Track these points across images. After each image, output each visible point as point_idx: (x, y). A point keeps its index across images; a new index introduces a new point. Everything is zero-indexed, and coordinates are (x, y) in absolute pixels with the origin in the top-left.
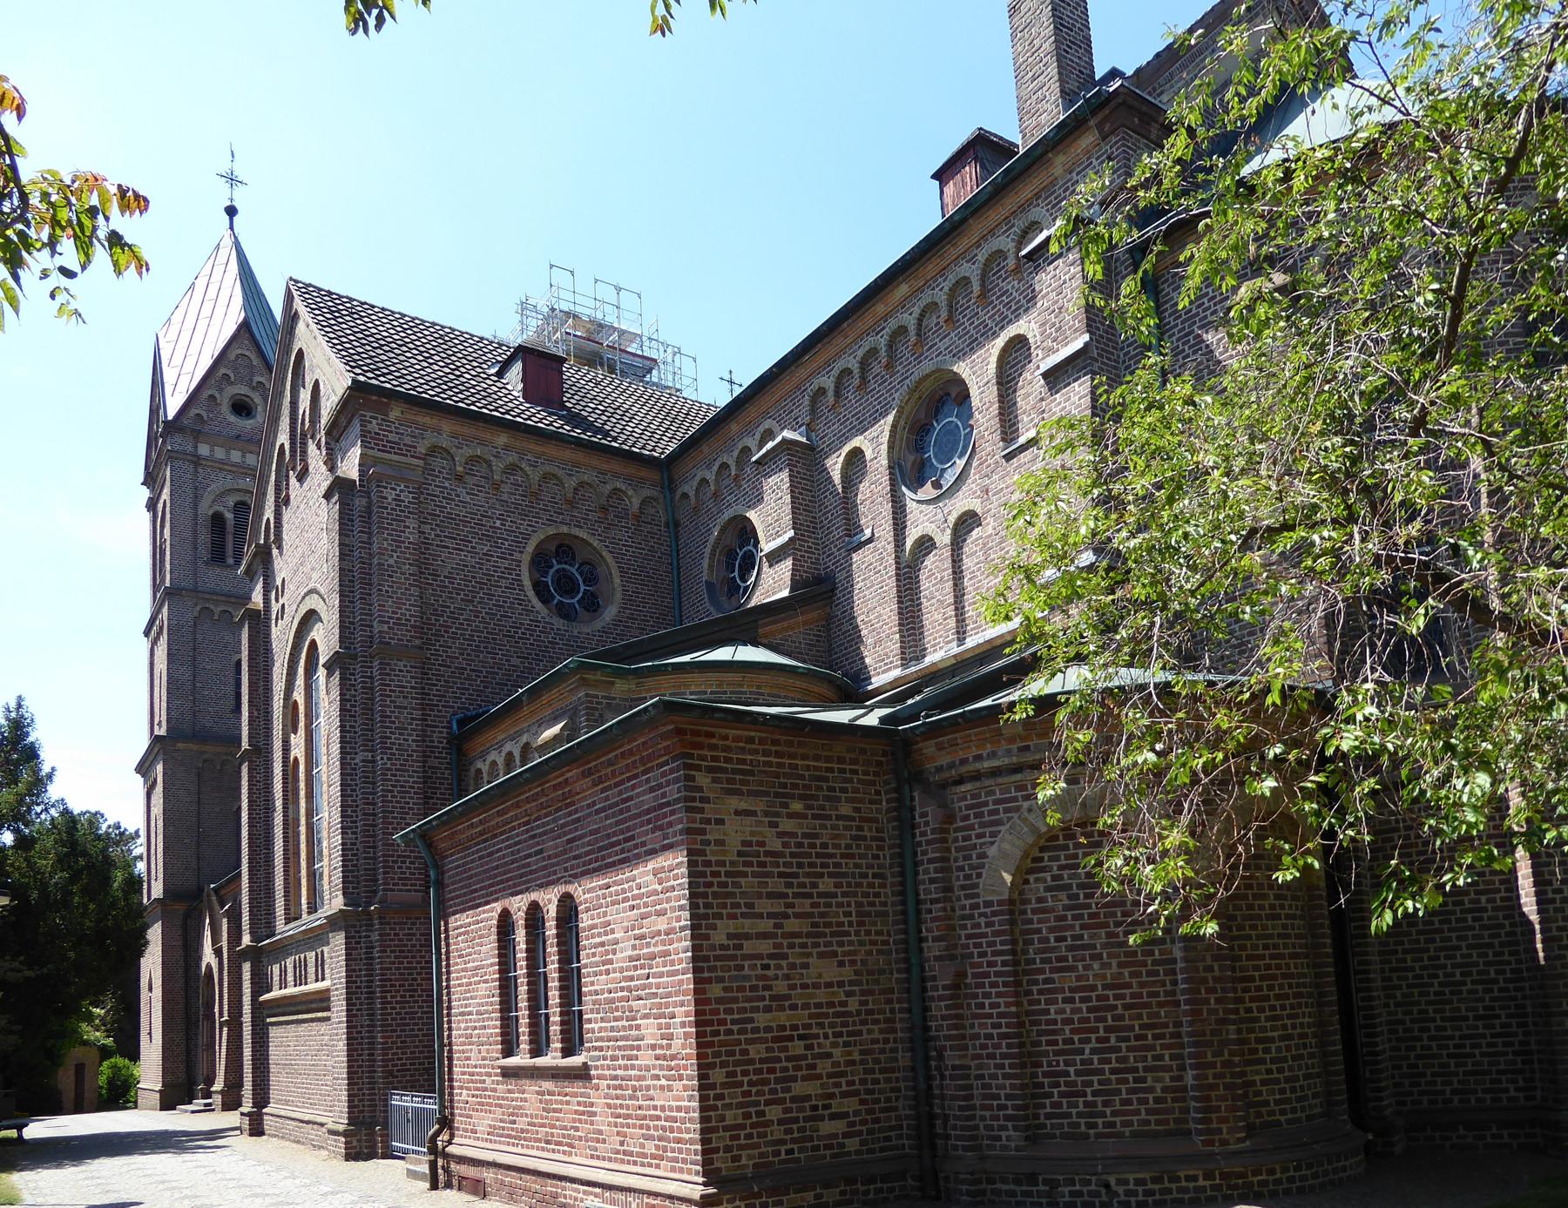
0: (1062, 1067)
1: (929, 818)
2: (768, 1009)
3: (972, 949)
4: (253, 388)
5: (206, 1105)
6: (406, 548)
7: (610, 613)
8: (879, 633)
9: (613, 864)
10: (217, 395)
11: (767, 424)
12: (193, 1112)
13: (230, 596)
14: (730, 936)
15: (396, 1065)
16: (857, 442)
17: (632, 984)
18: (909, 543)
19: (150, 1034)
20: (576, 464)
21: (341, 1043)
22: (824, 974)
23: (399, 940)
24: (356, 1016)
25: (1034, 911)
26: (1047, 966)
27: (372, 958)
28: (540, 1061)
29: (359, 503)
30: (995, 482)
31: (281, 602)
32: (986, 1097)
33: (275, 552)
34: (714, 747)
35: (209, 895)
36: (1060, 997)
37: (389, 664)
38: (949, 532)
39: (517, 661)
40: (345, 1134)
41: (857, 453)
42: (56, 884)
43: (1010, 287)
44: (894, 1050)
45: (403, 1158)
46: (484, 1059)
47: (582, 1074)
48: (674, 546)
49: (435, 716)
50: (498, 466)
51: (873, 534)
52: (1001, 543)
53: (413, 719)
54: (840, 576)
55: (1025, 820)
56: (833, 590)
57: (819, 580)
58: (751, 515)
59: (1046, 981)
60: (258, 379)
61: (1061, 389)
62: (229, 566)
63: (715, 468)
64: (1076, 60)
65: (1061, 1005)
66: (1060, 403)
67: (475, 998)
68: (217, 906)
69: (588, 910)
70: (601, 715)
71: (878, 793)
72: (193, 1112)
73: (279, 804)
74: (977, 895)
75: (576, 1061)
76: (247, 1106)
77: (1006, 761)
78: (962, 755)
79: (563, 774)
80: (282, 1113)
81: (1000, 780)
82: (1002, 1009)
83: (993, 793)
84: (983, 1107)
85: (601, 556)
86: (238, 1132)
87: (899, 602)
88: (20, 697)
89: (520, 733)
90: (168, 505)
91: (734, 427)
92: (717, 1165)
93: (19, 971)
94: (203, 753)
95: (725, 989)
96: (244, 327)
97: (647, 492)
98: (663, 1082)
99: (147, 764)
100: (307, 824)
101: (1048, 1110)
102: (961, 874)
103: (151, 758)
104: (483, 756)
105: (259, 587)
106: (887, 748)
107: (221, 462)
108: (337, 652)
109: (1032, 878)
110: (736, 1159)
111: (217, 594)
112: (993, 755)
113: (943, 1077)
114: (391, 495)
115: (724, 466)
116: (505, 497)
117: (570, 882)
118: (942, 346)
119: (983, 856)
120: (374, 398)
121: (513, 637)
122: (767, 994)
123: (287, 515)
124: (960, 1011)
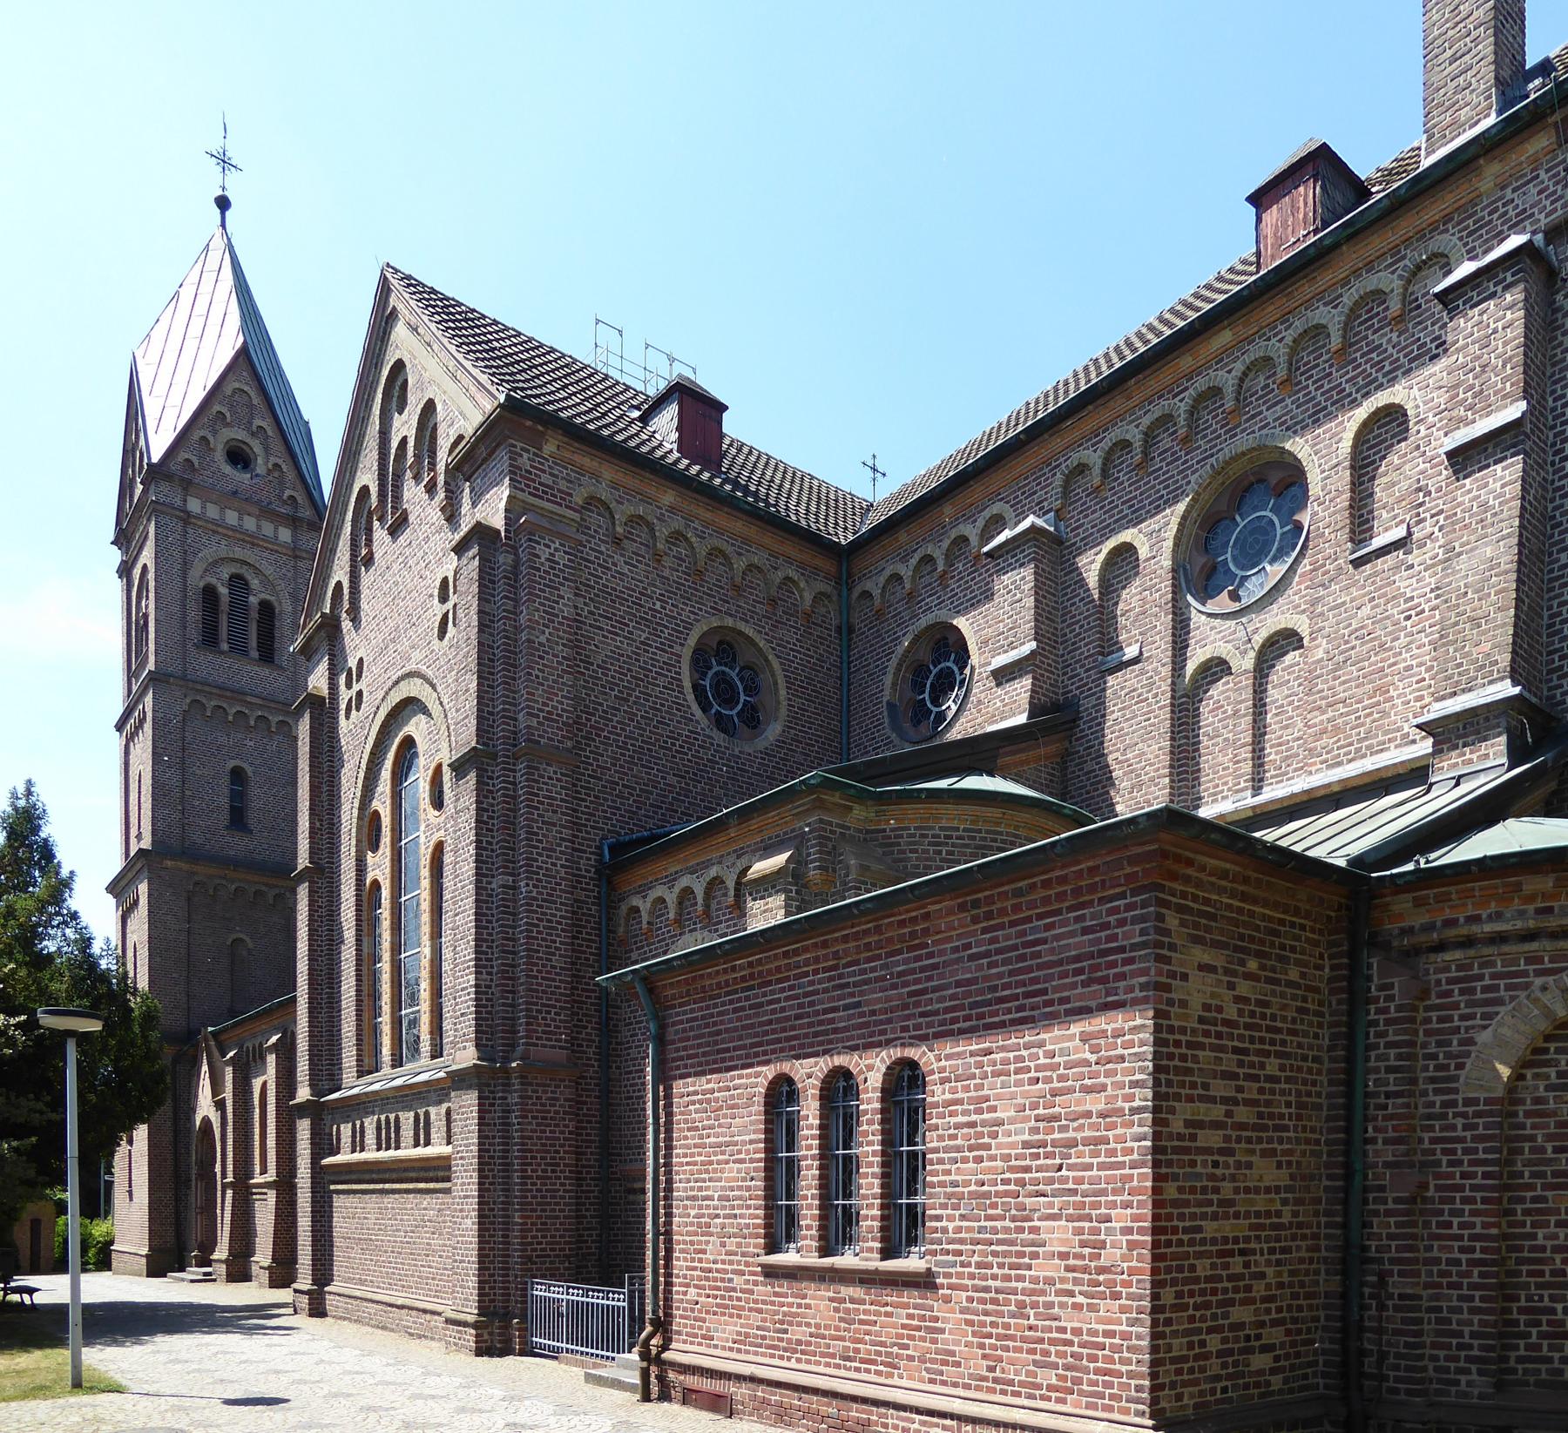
0: (1546, 1302)
1: (1396, 991)
2: (1215, 1217)
3: (1439, 1156)
4: (253, 434)
5: (205, 1274)
6: (559, 623)
7: (773, 731)
8: (1140, 775)
9: (1002, 1025)
10: (211, 439)
11: (996, 508)
14: (1189, 1124)
15: (536, 1250)
16: (1126, 536)
17: (1027, 1176)
18: (1191, 667)
21: (469, 1221)
22: (1265, 1178)
23: (542, 1105)
24: (489, 1190)
25: (1528, 1114)
26: (1539, 1182)
27: (508, 1124)
28: (846, 1260)
29: (504, 559)
30: (1336, 593)
31: (356, 687)
32: (1439, 1333)
33: (346, 625)
34: (1187, 880)
35: (206, 1040)
36: (1553, 1219)
37: (537, 769)
38: (1252, 654)
39: (672, 780)
40: (475, 1326)
41: (1126, 552)
43: (1384, 341)
44: (1317, 1272)
45: (556, 1358)
46: (728, 1253)
47: (924, 1282)
48: (845, 658)
49: (583, 838)
50: (662, 532)
51: (1141, 653)
52: (1336, 670)
53: (562, 839)
54: (1087, 703)
55: (1536, 1001)
56: (1075, 720)
57: (1056, 707)
58: (961, 623)
59: (1535, 1200)
60: (258, 422)
61: (1474, 472)
62: (222, 653)
63: (914, 561)
64: (1511, 39)
65: (1552, 1229)
66: (1470, 491)
67: (720, 1180)
68: (216, 1053)
69: (943, 1081)
70: (834, 848)
71: (1321, 957)
73: (349, 934)
74: (1456, 1091)
75: (912, 1262)
76: (304, 1282)
77: (1519, 924)
78: (1448, 914)
79: (924, 907)
80: (358, 1294)
81: (1506, 948)
82: (1478, 1230)
83: (1493, 964)
84: (1434, 1346)
85: (767, 660)
86: (291, 1311)
87: (1173, 739)
89: (707, 865)
90: (151, 576)
91: (948, 510)
92: (1163, 1404)
93: (41, 1113)
94: (194, 873)
95: (1181, 1190)
96: (243, 355)
97: (821, 586)
98: (1080, 1299)
100: (393, 961)
101: (1522, 1352)
102: (1432, 1064)
103: (130, 875)
104: (642, 891)
105: (322, 668)
106: (1343, 901)
107: (213, 522)
108: (474, 748)
109: (1529, 1073)
110: (1179, 1397)
112: (1498, 916)
113: (1382, 1307)
114: (544, 553)
115: (928, 559)
116: (666, 573)
117: (911, 1045)
118: (1270, 416)
119: (1471, 1042)
120: (529, 423)
121: (671, 750)
122: (1215, 1197)
123: (367, 579)
124: (1415, 1230)
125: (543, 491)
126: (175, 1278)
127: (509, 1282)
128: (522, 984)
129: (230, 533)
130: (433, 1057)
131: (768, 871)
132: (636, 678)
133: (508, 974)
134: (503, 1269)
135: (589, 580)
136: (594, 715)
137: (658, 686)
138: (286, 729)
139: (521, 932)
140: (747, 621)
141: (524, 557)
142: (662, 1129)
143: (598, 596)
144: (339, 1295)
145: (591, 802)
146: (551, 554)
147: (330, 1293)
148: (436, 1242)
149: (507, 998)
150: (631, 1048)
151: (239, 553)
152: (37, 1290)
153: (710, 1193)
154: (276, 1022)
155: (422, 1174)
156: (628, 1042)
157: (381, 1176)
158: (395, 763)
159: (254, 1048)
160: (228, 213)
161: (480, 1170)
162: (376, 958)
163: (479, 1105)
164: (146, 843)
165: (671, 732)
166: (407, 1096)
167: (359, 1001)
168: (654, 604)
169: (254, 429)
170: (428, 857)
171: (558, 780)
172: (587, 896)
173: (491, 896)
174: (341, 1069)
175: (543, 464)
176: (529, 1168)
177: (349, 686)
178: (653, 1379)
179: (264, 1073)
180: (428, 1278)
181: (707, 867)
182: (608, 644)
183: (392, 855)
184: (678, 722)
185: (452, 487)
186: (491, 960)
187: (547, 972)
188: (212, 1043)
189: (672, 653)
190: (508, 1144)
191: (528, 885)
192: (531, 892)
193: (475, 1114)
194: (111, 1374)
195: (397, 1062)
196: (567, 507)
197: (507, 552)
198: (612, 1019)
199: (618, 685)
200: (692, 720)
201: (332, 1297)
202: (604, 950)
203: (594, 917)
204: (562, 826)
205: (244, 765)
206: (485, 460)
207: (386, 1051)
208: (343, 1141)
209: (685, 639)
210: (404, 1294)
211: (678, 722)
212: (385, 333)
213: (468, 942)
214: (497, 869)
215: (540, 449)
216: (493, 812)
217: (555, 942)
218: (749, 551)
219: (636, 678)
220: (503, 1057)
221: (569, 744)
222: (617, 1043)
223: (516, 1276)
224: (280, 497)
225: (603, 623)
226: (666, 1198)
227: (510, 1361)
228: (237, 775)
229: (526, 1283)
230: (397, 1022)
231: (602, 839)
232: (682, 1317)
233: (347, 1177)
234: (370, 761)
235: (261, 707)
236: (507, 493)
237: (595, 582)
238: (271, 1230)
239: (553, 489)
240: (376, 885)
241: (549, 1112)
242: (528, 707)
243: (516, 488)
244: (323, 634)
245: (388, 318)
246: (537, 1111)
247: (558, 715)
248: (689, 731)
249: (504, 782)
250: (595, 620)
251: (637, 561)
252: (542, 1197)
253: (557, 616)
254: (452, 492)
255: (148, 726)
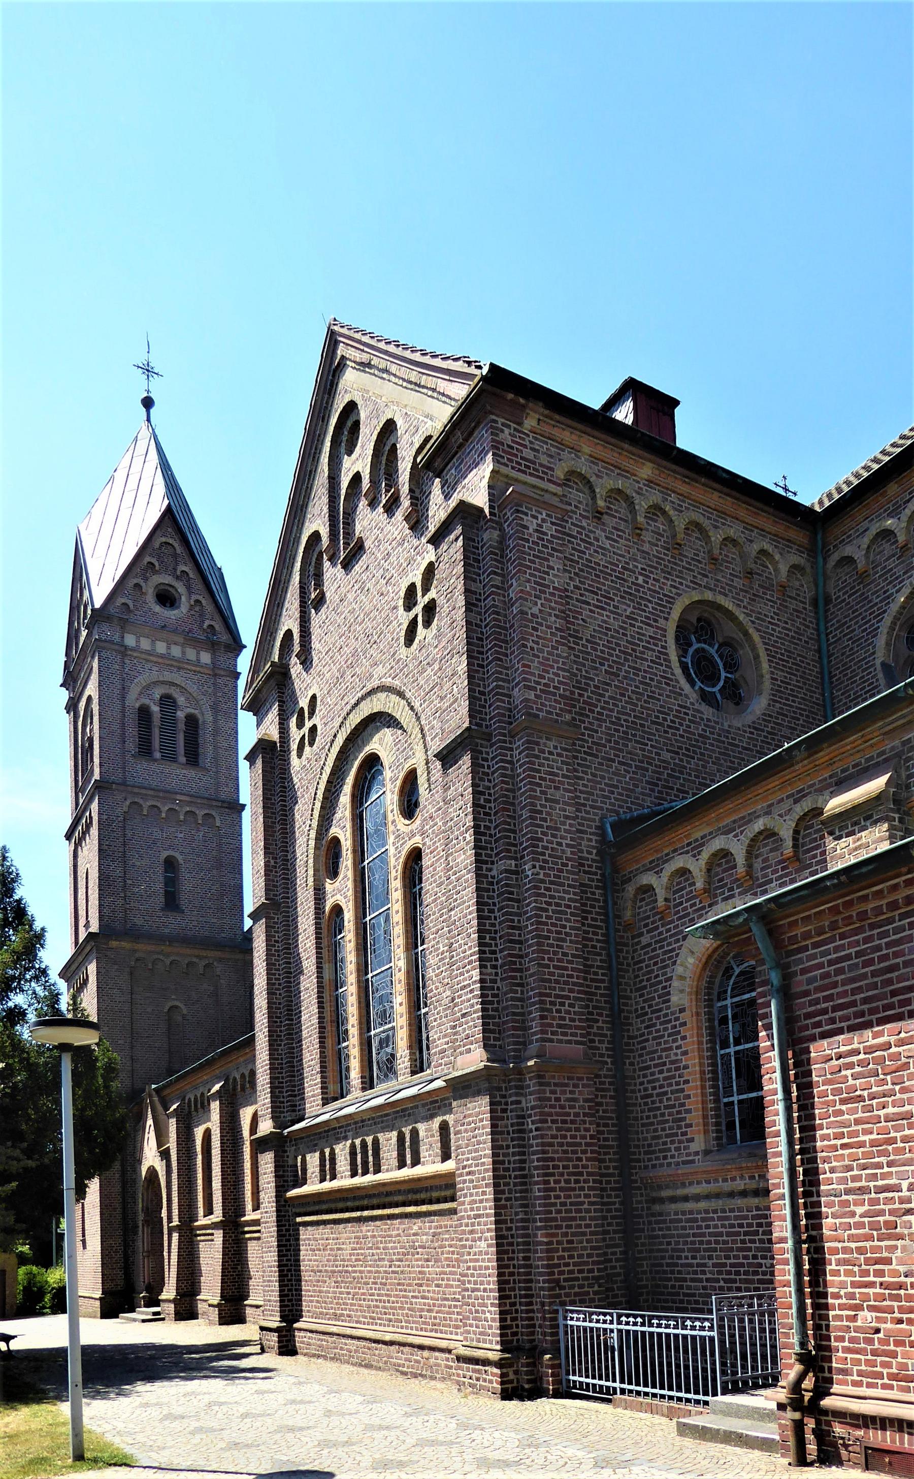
5: (155, 1314)
6: (550, 594)
7: (759, 705)
10: (143, 584)
12: (144, 1321)
13: (159, 791)
19: (84, 1242)
20: (723, 513)
21: (483, 1245)
24: (505, 1207)
29: (490, 536)
31: (308, 724)
33: (296, 669)
35: (150, 1096)
37: (538, 744)
39: (667, 756)
40: (499, 1364)
42: (46, 1063)
45: (609, 1401)
50: (642, 505)
53: (567, 817)
62: (156, 760)
68: (160, 1108)
72: (144, 1321)
73: (309, 963)
80: (334, 1329)
85: (746, 634)
88: (4, 847)
90: (95, 707)
93: (19, 1160)
94: (135, 951)
96: (168, 513)
97: (795, 559)
99: (74, 967)
103: (80, 959)
104: (655, 867)
111: (145, 788)
114: (532, 525)
116: (646, 547)
120: (511, 396)
123: (316, 619)
125: (526, 466)
126: (127, 1319)
127: (533, 1311)
128: (531, 975)
129: (160, 660)
130: (413, 1073)
131: (861, 800)
132: (624, 653)
133: (515, 966)
134: (526, 1296)
135: (573, 555)
136: (586, 690)
137: (646, 660)
138: (211, 820)
139: (528, 919)
140: (726, 595)
141: (509, 531)
142: (795, 1106)
143: (582, 571)
144: (311, 1331)
145: (588, 780)
146: (538, 525)
147: (300, 1330)
148: (431, 1270)
149: (516, 992)
150: (647, 1040)
151: (168, 676)
152: (13, 1337)
153: (893, 1181)
154: (217, 1072)
155: (410, 1197)
156: (643, 1035)
157: (357, 1203)
158: (355, 786)
159: (196, 1099)
160: (152, 411)
161: (496, 1185)
162: (338, 983)
163: (491, 1111)
164: (94, 928)
165: (661, 706)
166: (386, 1115)
167: (322, 1028)
168: (637, 579)
169: (178, 573)
170: (400, 868)
171: (559, 755)
172: (589, 879)
173: (492, 883)
174: (303, 1099)
175: (524, 439)
176: (552, 1179)
177: (300, 725)
178: (809, 1436)
179: (209, 1120)
180: (422, 1310)
181: (750, 821)
182: (595, 619)
183: (355, 876)
184: (668, 696)
185: (417, 494)
186: (494, 952)
187: (559, 960)
188: (156, 1099)
189: (657, 627)
190: (524, 1154)
191: (534, 867)
192: (538, 874)
193: (487, 1123)
194: (109, 1438)
195: (368, 1083)
196: (549, 481)
197: (493, 528)
198: (623, 1011)
199: (608, 660)
200: (681, 695)
201: (302, 1334)
202: (612, 935)
203: (598, 901)
204: (565, 803)
205: (177, 855)
206: (460, 446)
207: (355, 1075)
208: (309, 1172)
209: (669, 613)
210: (390, 1329)
211: (668, 696)
212: (331, 385)
213: (469, 936)
214: (497, 854)
215: (520, 424)
216: (490, 795)
217: (564, 927)
218: (724, 524)
219: (624, 653)
220: (515, 1057)
221: (568, 717)
222: (630, 1037)
223: (543, 1304)
224: (201, 627)
225: (589, 598)
226: (806, 1194)
227: (545, 1405)
228: (170, 864)
229: (557, 1312)
230: (366, 1044)
231: (601, 819)
232: (847, 1350)
233: (317, 1208)
234: (327, 790)
235: (190, 803)
236: (491, 467)
237: (579, 557)
238: (219, 1269)
239: (534, 463)
240: (338, 910)
241: (569, 1114)
242: (525, 679)
243: (498, 462)
244: (272, 682)
245: (335, 370)
246: (557, 1114)
247: (555, 687)
248: (679, 705)
249: (502, 761)
250: (581, 595)
251: (618, 536)
252: (567, 1211)
253: (548, 587)
254: (417, 499)
255: (94, 831)
